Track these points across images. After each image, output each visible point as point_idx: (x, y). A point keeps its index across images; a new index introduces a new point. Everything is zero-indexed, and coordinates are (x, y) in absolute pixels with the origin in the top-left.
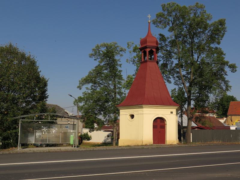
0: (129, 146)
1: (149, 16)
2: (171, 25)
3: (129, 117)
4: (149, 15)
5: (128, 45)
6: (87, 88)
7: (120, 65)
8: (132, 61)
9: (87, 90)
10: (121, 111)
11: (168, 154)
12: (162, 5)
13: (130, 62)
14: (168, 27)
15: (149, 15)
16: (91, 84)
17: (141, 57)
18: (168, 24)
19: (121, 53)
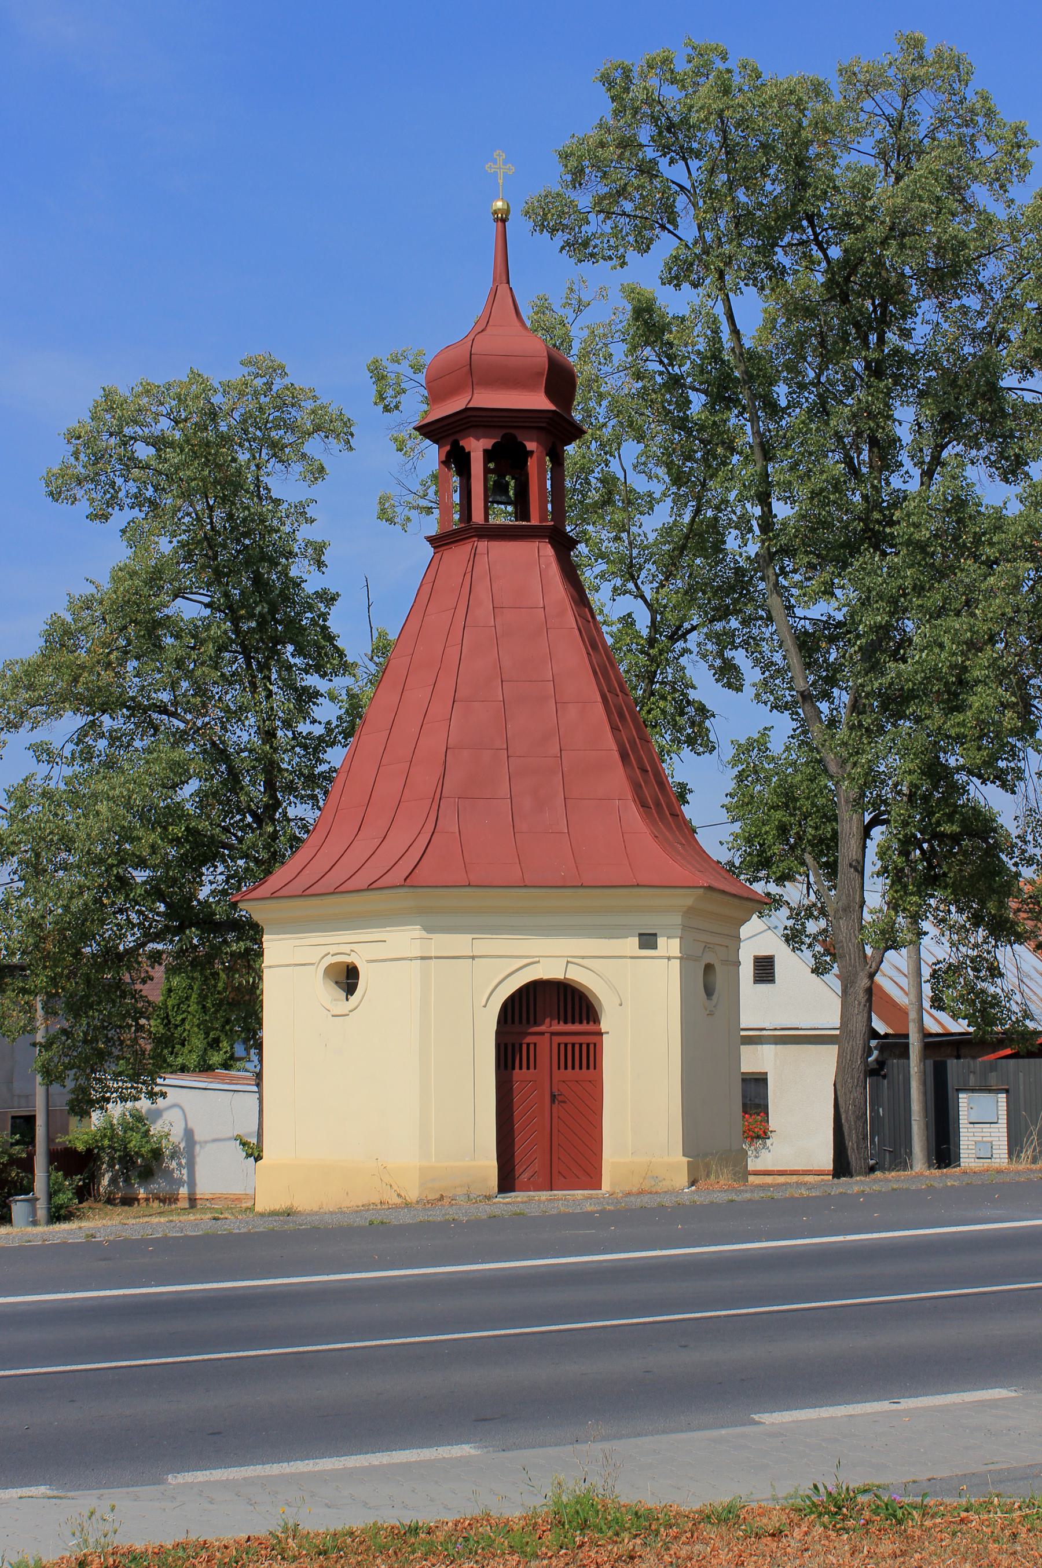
0: (289, 1213)
1: (500, 167)
2: (688, 229)
3: (329, 994)
4: (500, 155)
5: (380, 377)
6: (44, 752)
7: (318, 555)
8: (429, 510)
9: (43, 769)
10: (270, 942)
11: (124, 1296)
12: (607, 80)
13: (414, 514)
14: (665, 246)
15: (500, 155)
16: (71, 722)
17: (716, 332)
18: (670, 217)
19: (313, 446)
